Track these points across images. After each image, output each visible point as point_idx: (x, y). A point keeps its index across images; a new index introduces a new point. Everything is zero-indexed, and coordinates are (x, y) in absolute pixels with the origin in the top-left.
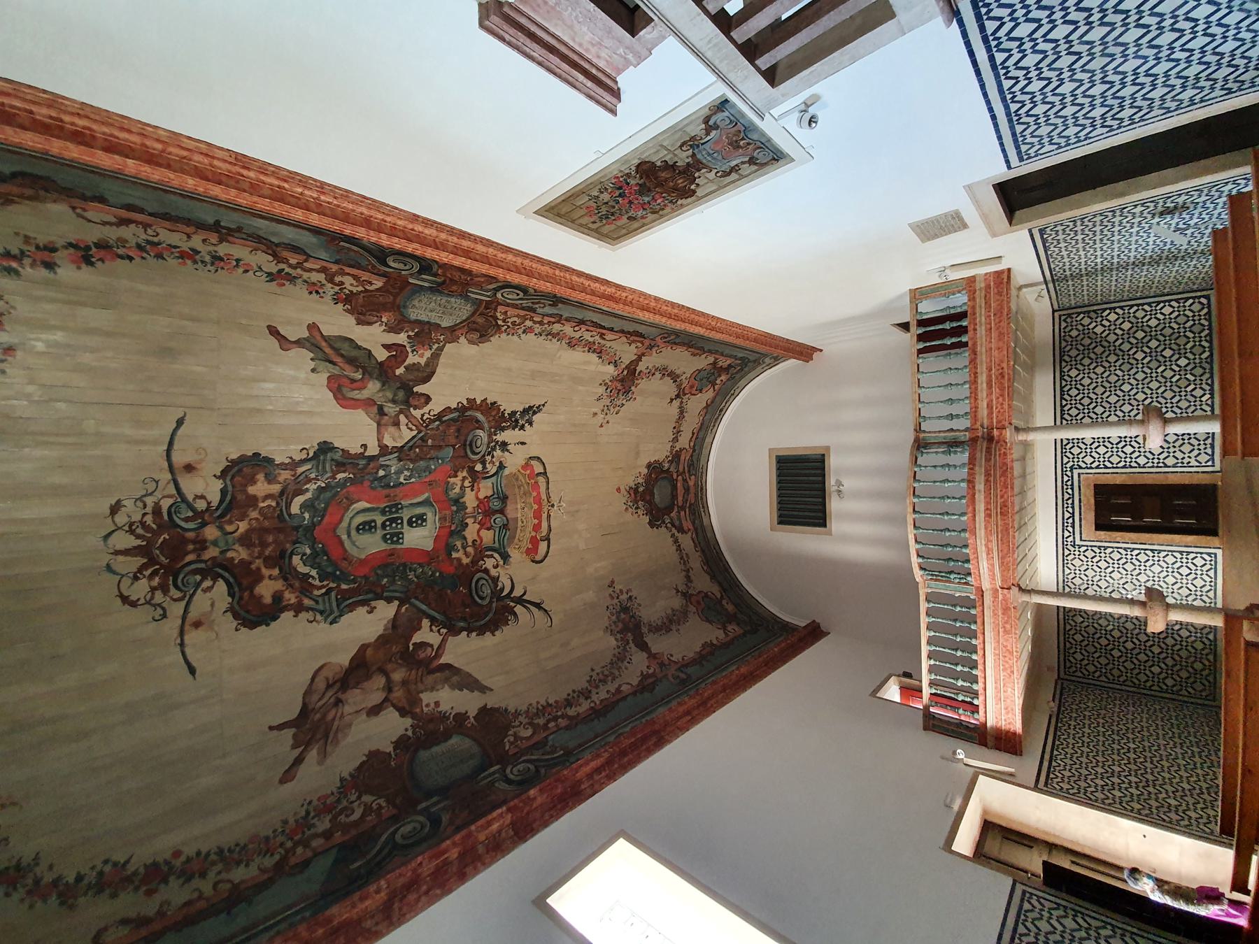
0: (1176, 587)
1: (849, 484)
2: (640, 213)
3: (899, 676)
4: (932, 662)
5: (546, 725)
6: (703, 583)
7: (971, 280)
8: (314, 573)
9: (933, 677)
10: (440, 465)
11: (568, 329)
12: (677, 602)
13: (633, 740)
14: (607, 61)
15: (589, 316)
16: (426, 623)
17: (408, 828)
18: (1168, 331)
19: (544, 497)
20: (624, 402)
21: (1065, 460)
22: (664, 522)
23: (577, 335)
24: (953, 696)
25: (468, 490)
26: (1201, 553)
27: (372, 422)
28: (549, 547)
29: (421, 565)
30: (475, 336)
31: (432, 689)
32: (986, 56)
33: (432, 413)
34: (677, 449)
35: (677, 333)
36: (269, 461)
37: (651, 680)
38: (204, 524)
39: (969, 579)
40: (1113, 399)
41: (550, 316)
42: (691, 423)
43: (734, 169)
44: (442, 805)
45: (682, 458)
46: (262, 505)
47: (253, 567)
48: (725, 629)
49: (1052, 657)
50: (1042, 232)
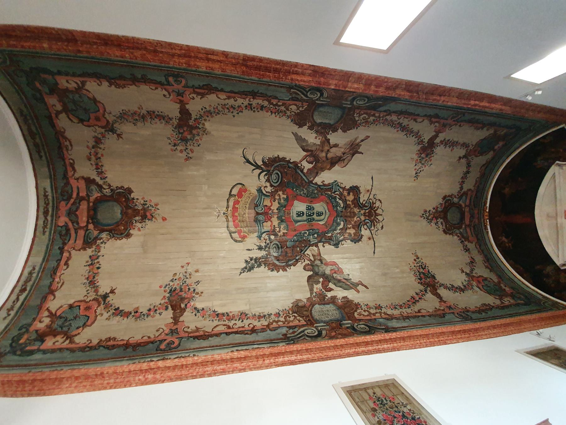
5: (282, 105)
8: (338, 200)
16: (305, 171)
20: (171, 284)
25: (277, 226)
28: (231, 191)
31: (315, 144)
33: (301, 262)
36: (352, 241)
38: (364, 221)
45: (81, 242)
46: (351, 226)
47: (353, 205)
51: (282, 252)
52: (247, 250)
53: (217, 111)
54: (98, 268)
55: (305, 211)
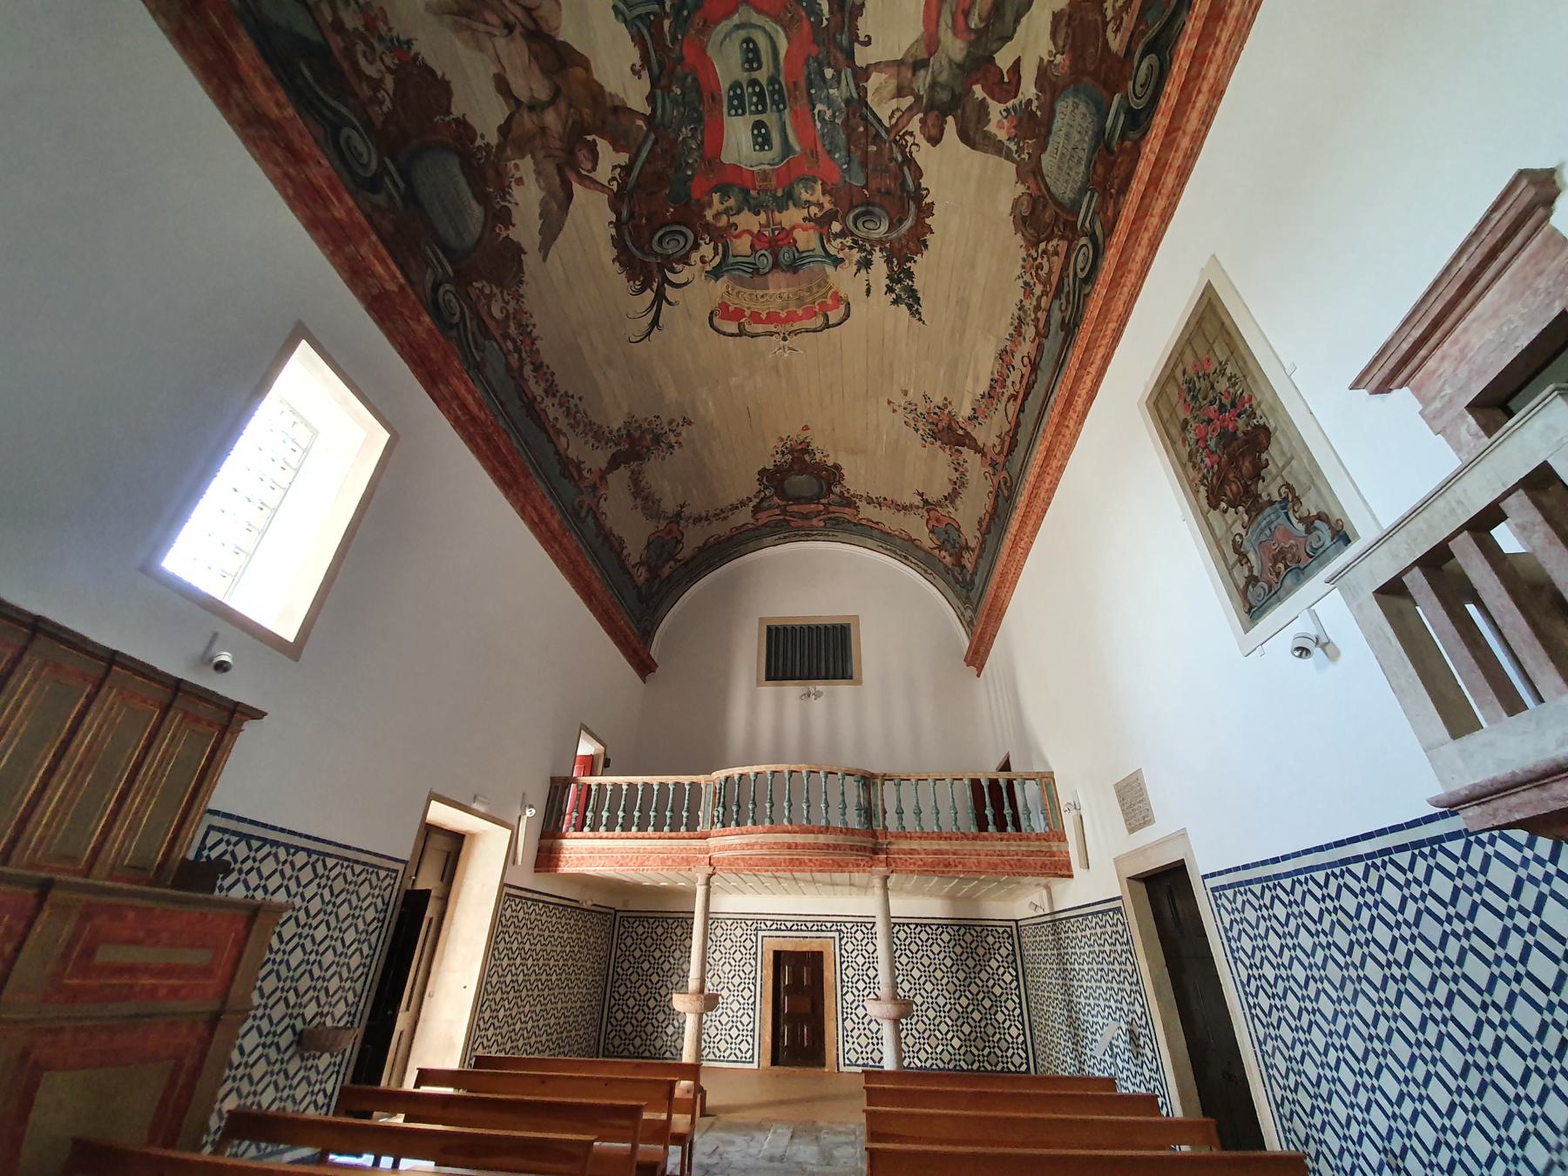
0: (717, 1023)
1: (818, 706)
2: (1192, 436)
3: (605, 754)
4: (625, 787)
6: (694, 538)
7: (1062, 838)
9: (609, 788)
10: (841, 167)
11: (1027, 347)
12: (669, 506)
13: (504, 450)
14: (1434, 372)
15: (1043, 378)
16: (623, 158)
17: (361, 148)
18: (990, 1030)
19: (797, 326)
20: (921, 432)
21: (849, 925)
22: (766, 488)
23: (1017, 362)
24: (591, 807)
25: (805, 213)
26: (753, 1049)
27: (903, 53)
28: (732, 335)
29: (701, 145)
30: (1025, 210)
31: (538, 173)
32: (1362, 852)
34: (858, 503)
35: (1010, 499)
37: (576, 475)
39: (719, 825)
40: (916, 973)
41: (1048, 322)
42: (890, 520)
43: (1243, 557)
44: (395, 194)
45: (847, 510)
48: (641, 564)
49: (636, 905)
50: (1117, 910)
51: (881, 206)
52: (868, 295)
53: (588, 428)
54: (885, 499)
55: (750, 119)
